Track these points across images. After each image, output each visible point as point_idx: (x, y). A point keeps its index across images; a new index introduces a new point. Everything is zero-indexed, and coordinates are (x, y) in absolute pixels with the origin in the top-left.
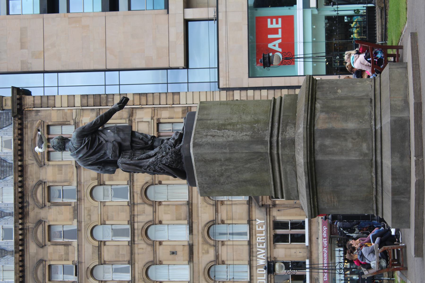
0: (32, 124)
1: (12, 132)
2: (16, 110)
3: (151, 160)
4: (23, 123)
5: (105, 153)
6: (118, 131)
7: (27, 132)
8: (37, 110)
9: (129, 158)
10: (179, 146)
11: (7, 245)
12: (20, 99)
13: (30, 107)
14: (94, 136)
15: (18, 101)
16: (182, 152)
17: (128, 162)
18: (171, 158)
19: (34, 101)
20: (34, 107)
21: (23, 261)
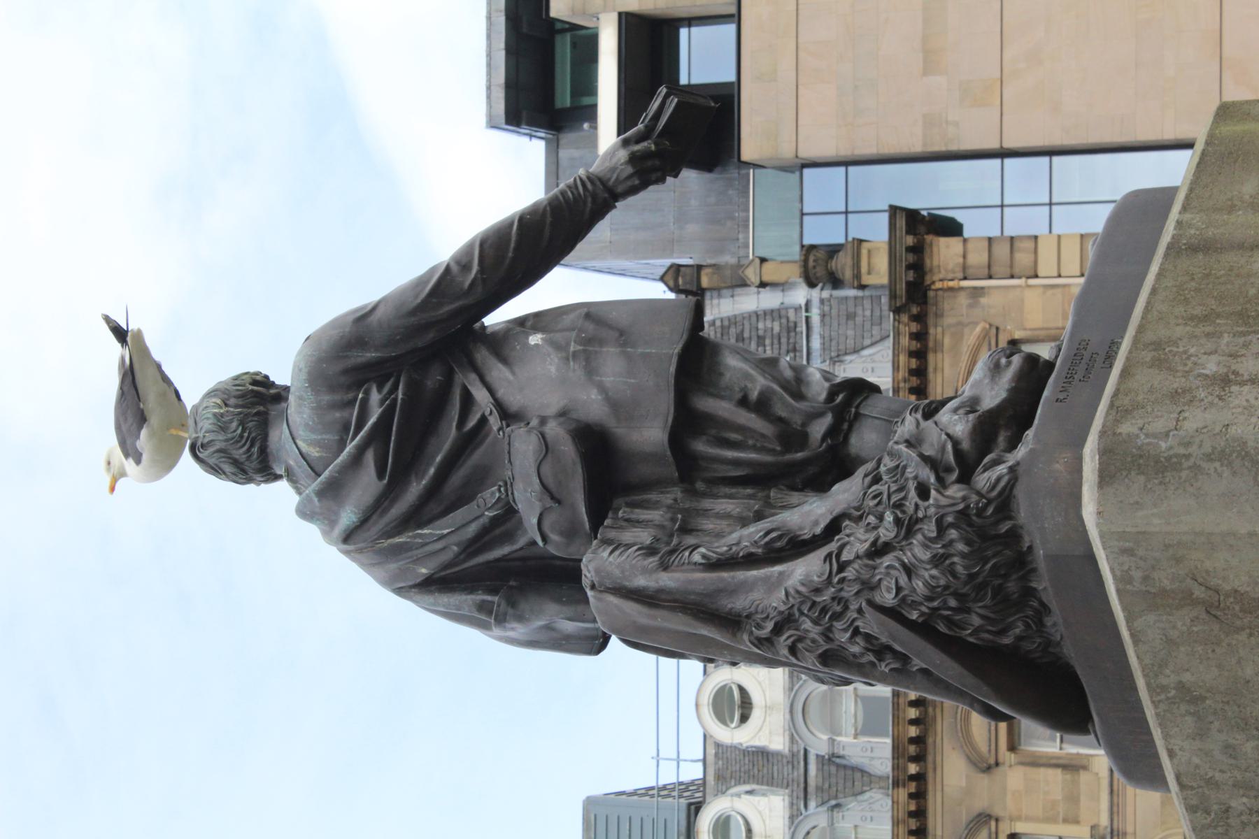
0: (958, 337)
1: (889, 366)
2: (901, 288)
3: (805, 570)
4: (926, 333)
5: (509, 512)
6: (589, 341)
7: (940, 365)
8: (975, 288)
9: (650, 551)
10: (1002, 469)
11: (868, 754)
12: (918, 250)
13: (950, 276)
14: (433, 379)
15: (911, 258)
16: (1022, 512)
17: (641, 582)
18: (937, 561)
19: (964, 257)
20: (965, 278)
21: (920, 814)
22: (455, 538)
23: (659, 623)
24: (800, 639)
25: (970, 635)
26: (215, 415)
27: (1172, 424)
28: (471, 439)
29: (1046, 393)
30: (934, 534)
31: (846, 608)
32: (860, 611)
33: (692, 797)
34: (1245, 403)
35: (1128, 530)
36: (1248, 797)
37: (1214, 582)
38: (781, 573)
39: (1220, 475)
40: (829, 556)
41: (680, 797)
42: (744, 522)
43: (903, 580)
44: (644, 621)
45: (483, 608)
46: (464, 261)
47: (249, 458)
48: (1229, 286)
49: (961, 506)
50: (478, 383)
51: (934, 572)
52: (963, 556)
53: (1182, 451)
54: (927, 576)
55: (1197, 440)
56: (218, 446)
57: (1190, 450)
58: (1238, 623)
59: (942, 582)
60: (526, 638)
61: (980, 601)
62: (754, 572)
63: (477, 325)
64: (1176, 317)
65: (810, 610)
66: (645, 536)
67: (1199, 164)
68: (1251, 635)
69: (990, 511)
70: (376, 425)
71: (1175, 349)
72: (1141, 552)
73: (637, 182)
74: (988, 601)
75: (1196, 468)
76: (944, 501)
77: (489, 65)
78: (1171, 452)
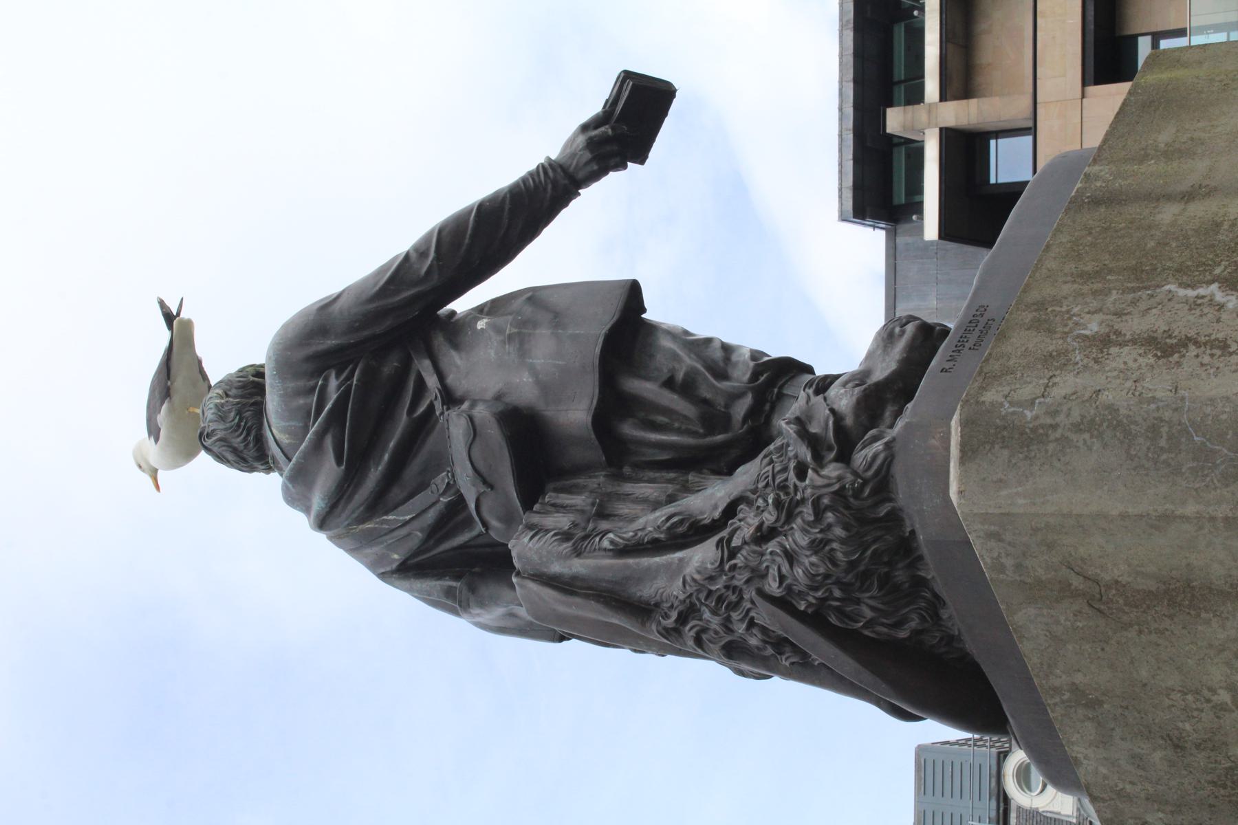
3: (703, 555)
9: (566, 536)
10: (878, 446)
14: (390, 366)
17: (556, 568)
22: (416, 524)
23: (572, 611)
24: (704, 630)
25: (864, 627)
26: (216, 405)
27: (1039, 391)
28: (424, 425)
29: (933, 363)
30: (811, 518)
31: (741, 598)
32: (753, 602)
33: (1002, 747)
34: (1122, 366)
35: (990, 511)
36: (1163, 812)
37: (1091, 571)
38: (681, 560)
39: (1090, 449)
40: (721, 541)
41: (991, 747)
42: (656, 505)
43: (785, 569)
44: (562, 609)
45: (449, 593)
46: (423, 248)
47: (246, 446)
48: (1127, 240)
49: (836, 487)
50: (431, 368)
51: (814, 559)
52: (843, 542)
53: (1049, 421)
54: (807, 564)
55: (1065, 408)
56: (219, 435)
57: (1058, 419)
58: (1125, 618)
59: (822, 570)
60: (496, 624)
61: (868, 590)
62: (657, 559)
63: (443, 311)
64: (1066, 275)
65: (706, 599)
66: (563, 521)
67: (1118, 113)
68: (1140, 632)
69: (867, 491)
70: (331, 410)
71: (1058, 309)
72: (1008, 537)
73: (595, 167)
74: (874, 592)
75: (1064, 441)
76: (819, 481)
77: (841, 172)
78: (1037, 423)
